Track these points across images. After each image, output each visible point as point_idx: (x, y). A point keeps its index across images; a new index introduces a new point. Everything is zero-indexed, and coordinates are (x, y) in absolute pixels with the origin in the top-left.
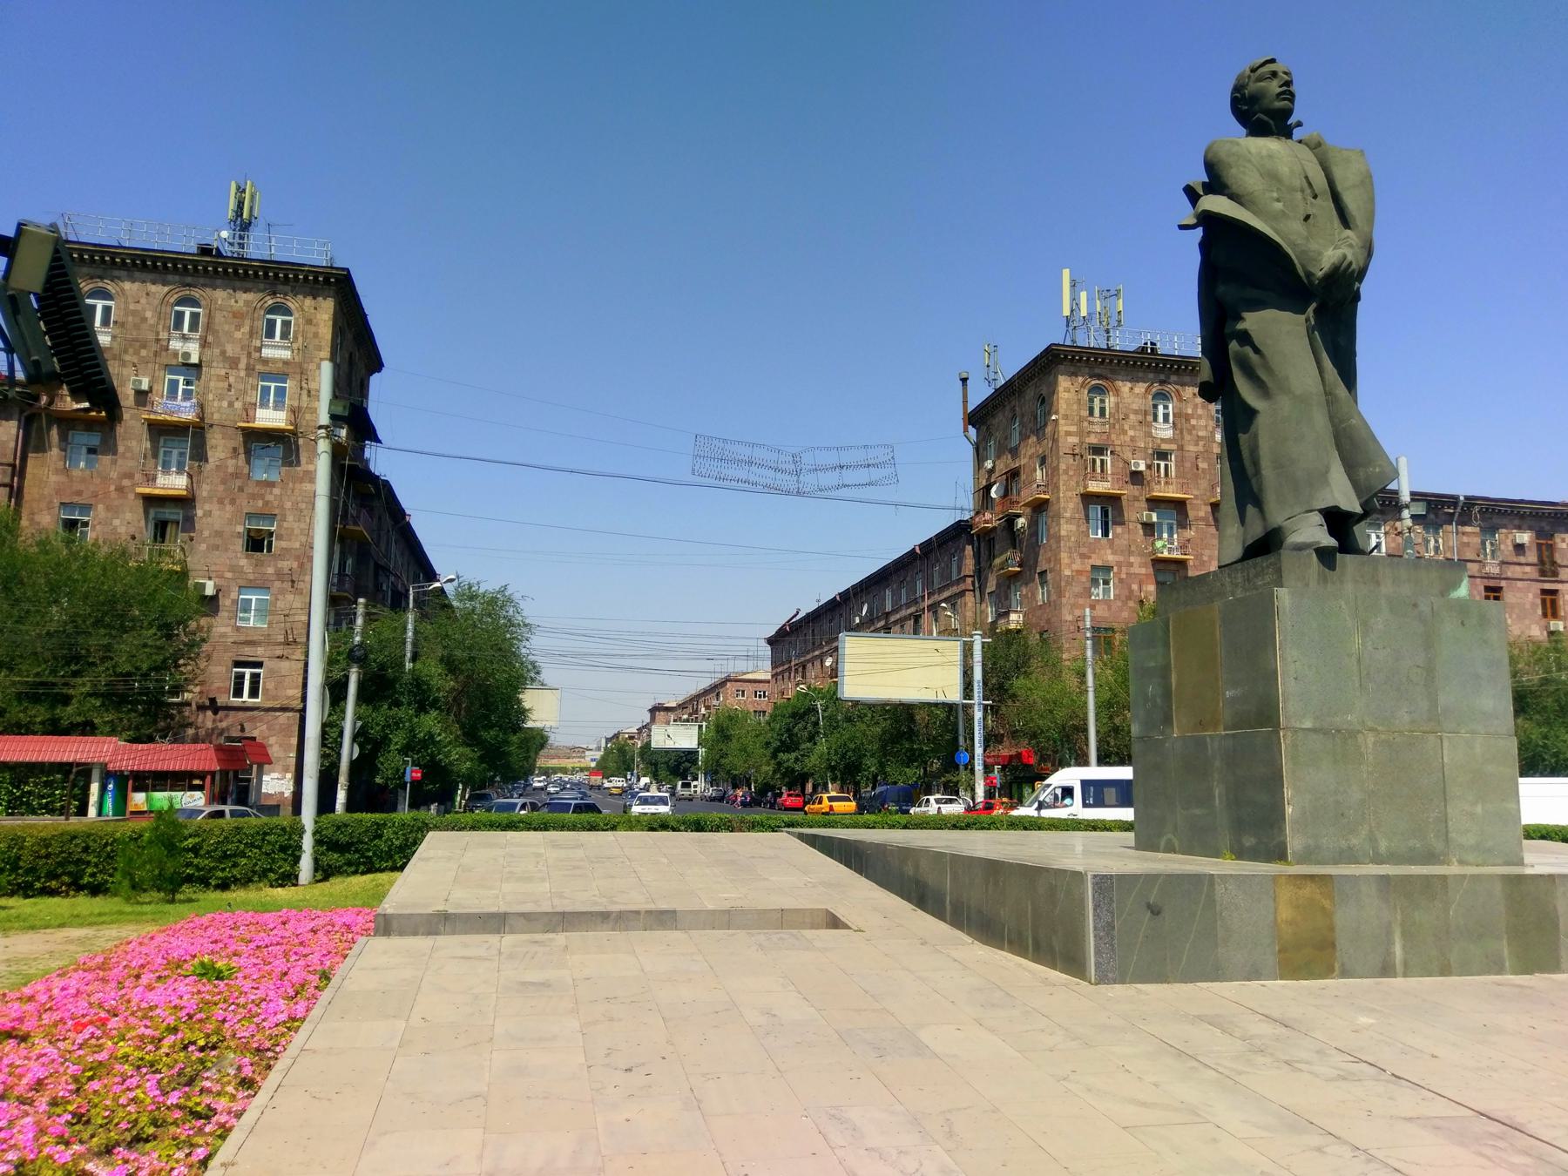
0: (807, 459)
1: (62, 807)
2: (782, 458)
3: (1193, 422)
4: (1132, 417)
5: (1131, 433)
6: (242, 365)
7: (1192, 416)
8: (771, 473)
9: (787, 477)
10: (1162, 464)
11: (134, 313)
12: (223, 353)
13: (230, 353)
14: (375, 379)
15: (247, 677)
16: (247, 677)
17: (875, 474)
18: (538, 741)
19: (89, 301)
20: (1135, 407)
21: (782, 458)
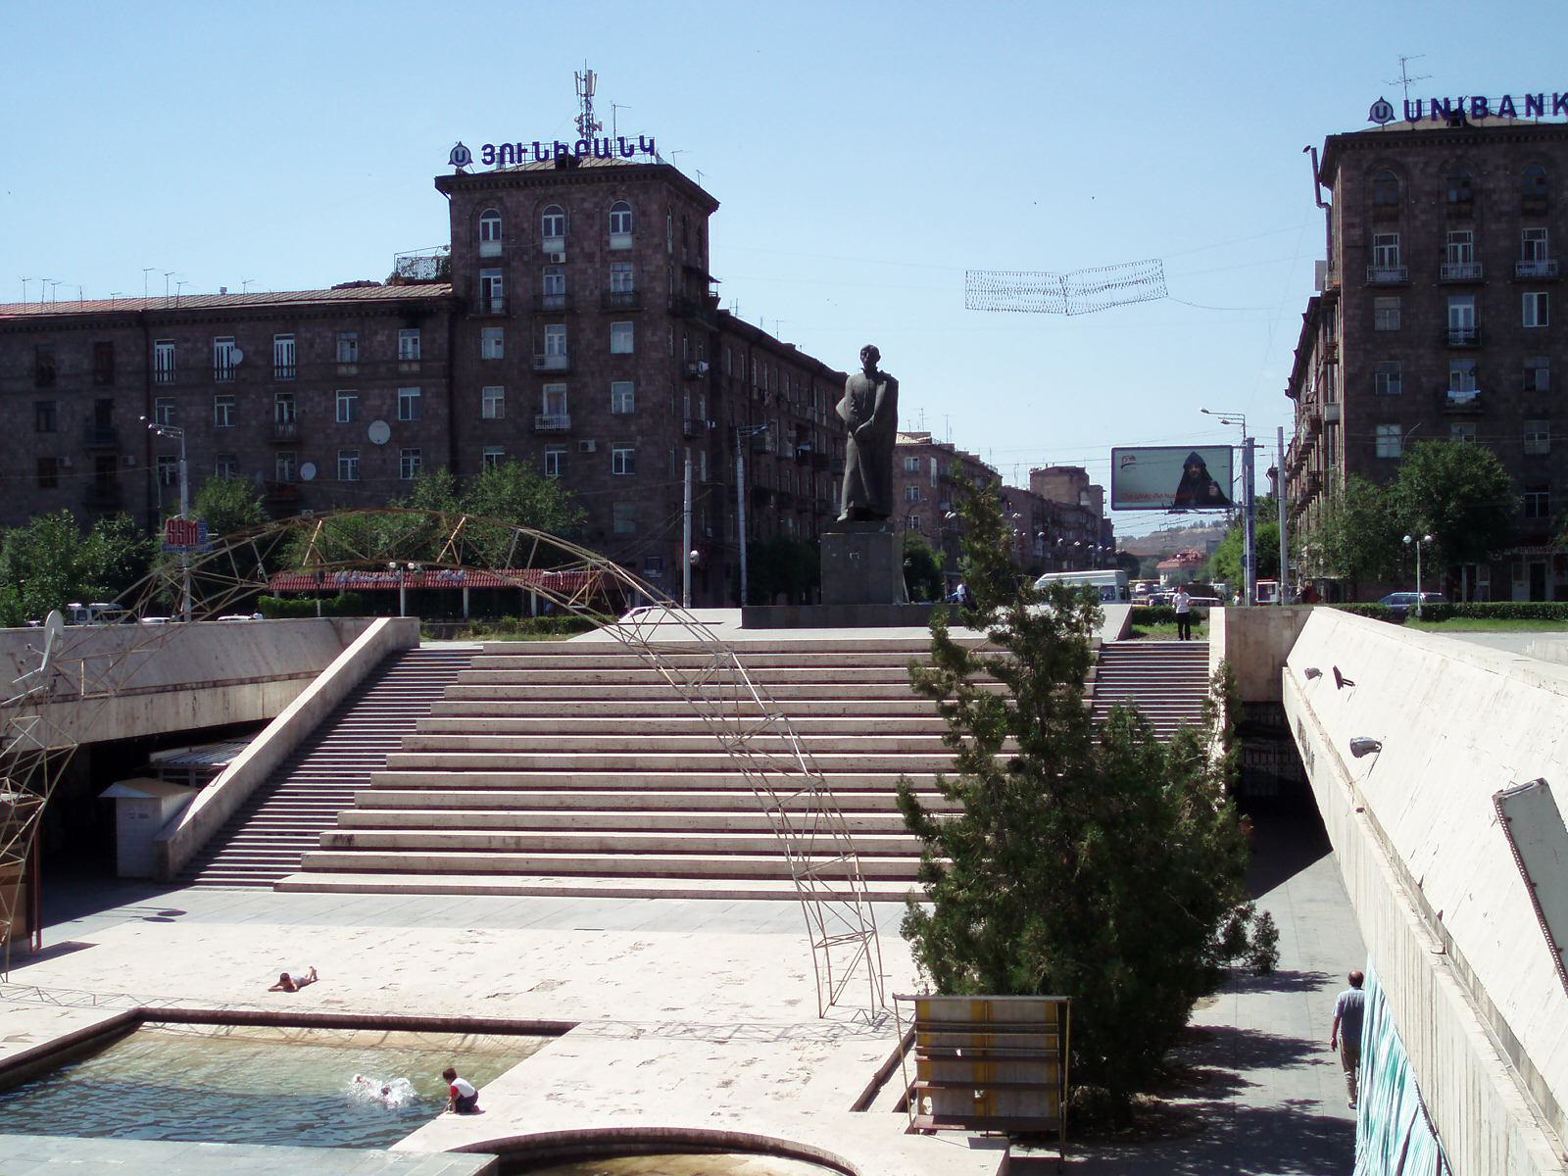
0: (1075, 282)
2: (1050, 279)
3: (1495, 197)
4: (1424, 199)
5: (1423, 217)
6: (597, 259)
7: (1494, 191)
8: (1040, 297)
9: (1056, 298)
10: (1460, 247)
11: (516, 226)
12: (582, 249)
13: (587, 250)
14: (712, 218)
15: (1386, 252)
16: (1386, 252)
17: (1143, 288)
18: (1273, 532)
20: (1427, 188)
21: (1050, 279)
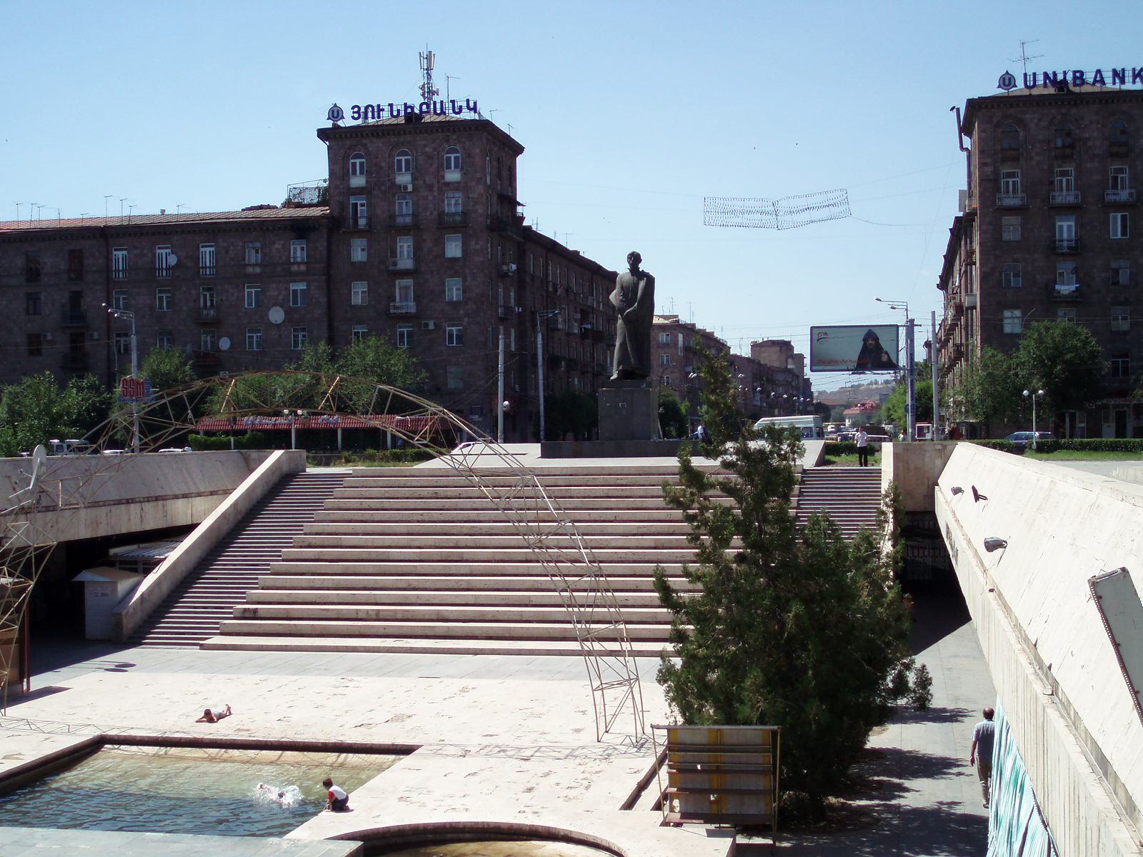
0: (783, 205)
1: (750, 597)
2: (765, 204)
3: (1090, 144)
4: (1038, 145)
5: (1037, 158)
6: (435, 189)
7: (1089, 139)
8: (758, 216)
9: (770, 217)
11: (376, 164)
12: (424, 182)
13: (428, 182)
15: (1011, 184)
16: (1011, 184)
17: (833, 210)
18: (928, 388)
19: (675, 790)
20: (1040, 137)
21: (765, 204)
